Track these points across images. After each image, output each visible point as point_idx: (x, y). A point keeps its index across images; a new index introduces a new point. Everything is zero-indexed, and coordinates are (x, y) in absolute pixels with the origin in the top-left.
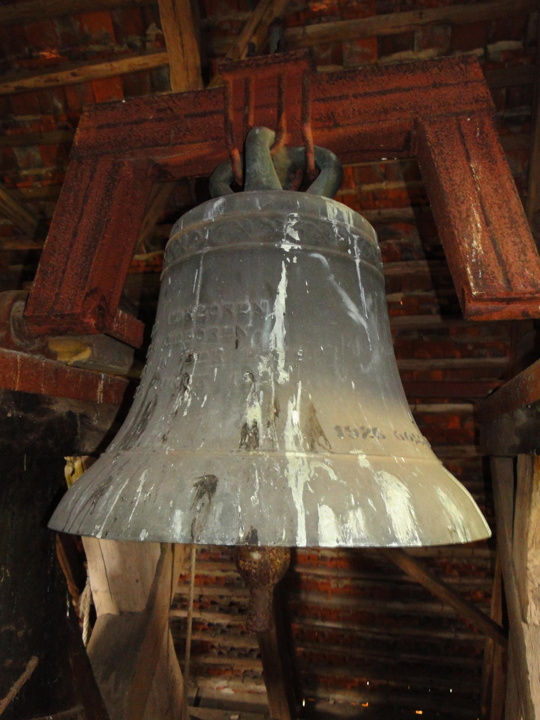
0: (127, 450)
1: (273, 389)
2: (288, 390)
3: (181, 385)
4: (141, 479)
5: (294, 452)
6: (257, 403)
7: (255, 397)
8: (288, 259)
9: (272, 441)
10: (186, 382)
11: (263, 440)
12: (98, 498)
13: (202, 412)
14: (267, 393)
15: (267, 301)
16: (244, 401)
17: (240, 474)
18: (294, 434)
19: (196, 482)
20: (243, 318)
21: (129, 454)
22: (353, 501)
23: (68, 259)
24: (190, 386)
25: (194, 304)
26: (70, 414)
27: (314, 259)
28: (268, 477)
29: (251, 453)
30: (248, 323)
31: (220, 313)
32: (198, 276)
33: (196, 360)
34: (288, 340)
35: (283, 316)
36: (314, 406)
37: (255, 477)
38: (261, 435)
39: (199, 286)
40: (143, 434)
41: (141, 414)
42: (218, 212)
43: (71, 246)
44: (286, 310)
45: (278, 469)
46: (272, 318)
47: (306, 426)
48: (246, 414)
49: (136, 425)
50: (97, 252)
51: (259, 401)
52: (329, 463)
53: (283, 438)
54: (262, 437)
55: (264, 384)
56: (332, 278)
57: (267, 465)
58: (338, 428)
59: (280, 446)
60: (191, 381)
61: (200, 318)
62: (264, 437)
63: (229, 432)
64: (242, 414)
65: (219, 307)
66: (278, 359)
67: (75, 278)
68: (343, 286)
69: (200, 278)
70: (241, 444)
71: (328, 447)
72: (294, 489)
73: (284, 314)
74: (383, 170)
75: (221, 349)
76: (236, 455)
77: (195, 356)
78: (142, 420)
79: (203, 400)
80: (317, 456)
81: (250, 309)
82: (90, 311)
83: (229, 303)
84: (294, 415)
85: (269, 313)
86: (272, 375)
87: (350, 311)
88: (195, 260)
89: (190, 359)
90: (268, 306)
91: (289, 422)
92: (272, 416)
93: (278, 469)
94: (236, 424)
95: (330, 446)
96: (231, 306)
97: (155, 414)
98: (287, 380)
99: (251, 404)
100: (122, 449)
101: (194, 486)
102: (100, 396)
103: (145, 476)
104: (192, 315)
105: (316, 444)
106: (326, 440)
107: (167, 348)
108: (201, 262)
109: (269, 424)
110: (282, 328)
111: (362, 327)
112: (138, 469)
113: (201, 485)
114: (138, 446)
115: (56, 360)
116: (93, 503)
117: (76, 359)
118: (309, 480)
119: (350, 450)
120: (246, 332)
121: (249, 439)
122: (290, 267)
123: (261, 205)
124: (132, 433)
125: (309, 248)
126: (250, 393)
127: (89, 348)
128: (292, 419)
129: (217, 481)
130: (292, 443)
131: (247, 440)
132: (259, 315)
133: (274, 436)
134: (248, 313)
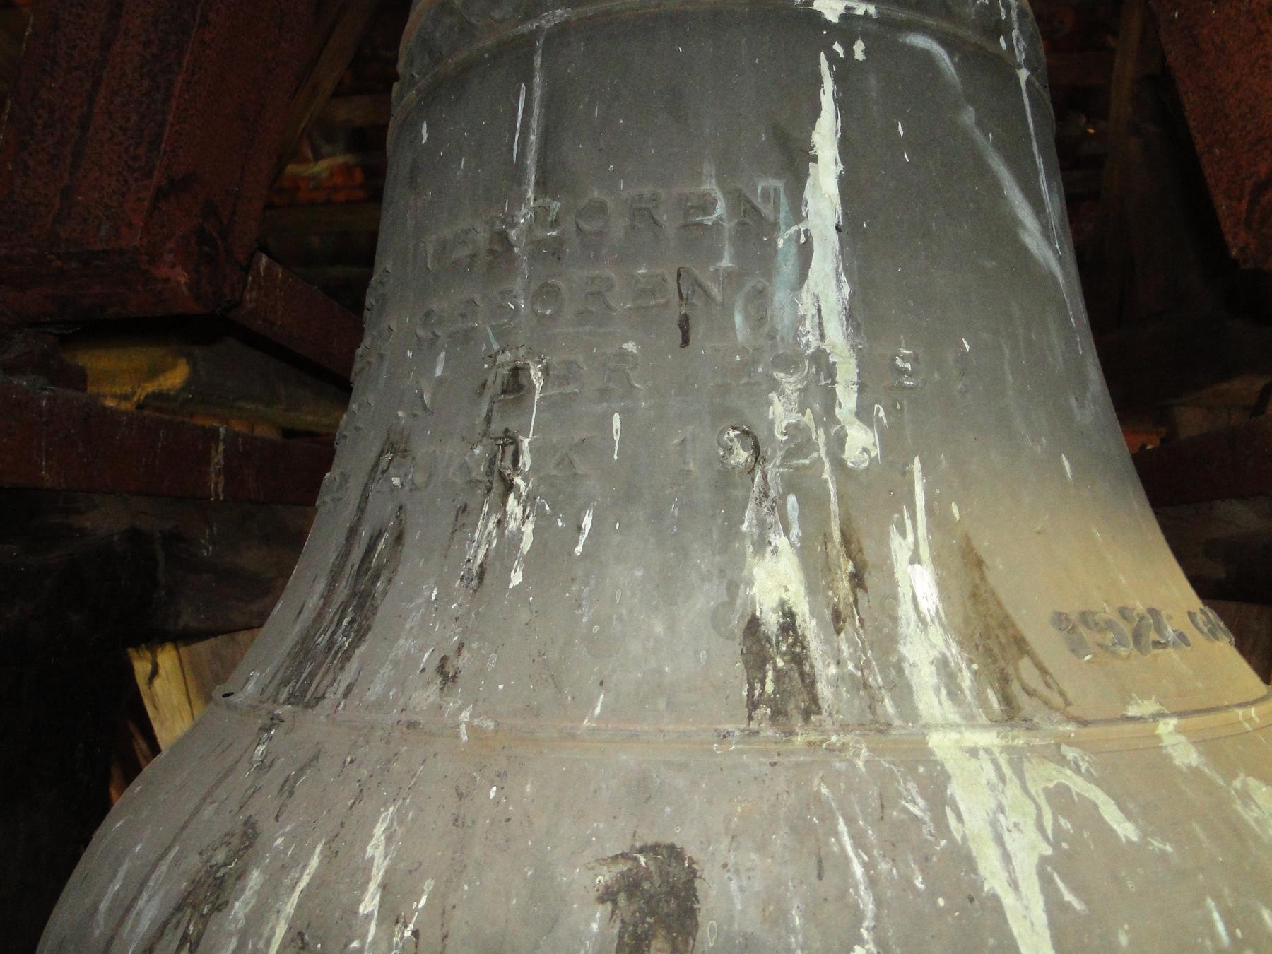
0: (308, 706)
1: (831, 487)
2: (879, 492)
3: (490, 472)
4: (370, 851)
5: (953, 726)
6: (780, 541)
7: (770, 519)
8: (837, 47)
9: (866, 686)
10: (508, 463)
11: (829, 682)
12: (205, 919)
13: (579, 573)
14: (813, 502)
15: (779, 184)
16: (731, 530)
17: (780, 839)
18: (935, 653)
19: (604, 877)
20: (697, 237)
21: (314, 725)
22: (1220, 927)
24: (526, 479)
25: (522, 199)
26: (135, 536)
27: (913, 50)
28: (892, 848)
29: (799, 740)
30: (719, 257)
31: (618, 226)
32: (529, 104)
33: (538, 385)
34: (860, 316)
35: (834, 236)
36: (975, 543)
37: (843, 850)
38: (819, 665)
39: (533, 138)
40: (363, 648)
41: (348, 572)
44: (845, 214)
45: (918, 808)
46: (802, 240)
47: (967, 620)
48: (750, 583)
49: (332, 609)
50: (185, 64)
52: (1084, 767)
53: (900, 671)
54: (825, 671)
55: (797, 468)
56: (969, 116)
57: (873, 792)
58: (1060, 619)
59: (897, 705)
60: (526, 460)
61: (544, 242)
62: (833, 670)
63: (697, 652)
64: (735, 584)
65: (611, 206)
66: (834, 383)
67: (120, 143)
68: (999, 147)
69: (536, 111)
70: (753, 705)
71: (1058, 701)
72: (1008, 899)
73: (838, 229)
75: (630, 347)
76: (741, 752)
77: (536, 374)
78: (353, 595)
79: (579, 528)
80: (1037, 742)
81: (720, 209)
82: (171, 245)
83: (647, 190)
84: (918, 583)
85: (789, 227)
86: (820, 437)
87: (1024, 227)
88: (515, 56)
89: (516, 383)
90: (783, 200)
91: (905, 610)
92: (844, 586)
93: (918, 808)
94: (717, 619)
95: (1062, 693)
96: (655, 199)
97: (401, 579)
98: (875, 452)
99: (762, 544)
100: (287, 701)
101: (602, 900)
102: (216, 484)
103: (389, 840)
104: (513, 234)
105: (1015, 687)
106: (1043, 671)
107: (427, 348)
108: (538, 60)
109: (837, 616)
110: (837, 274)
111: (1054, 277)
112: (358, 799)
113: (630, 896)
114: (345, 696)
115: (84, 390)
116: (185, 937)
117: (150, 388)
118: (1048, 851)
119: (1126, 703)
120: (715, 290)
121: (777, 680)
122: (845, 71)
124: (322, 640)
125: (902, 15)
126: (752, 504)
127: (183, 361)
128: (914, 598)
129: (693, 873)
130: (937, 691)
131: (770, 687)
132: (755, 229)
133: (868, 664)
134: (717, 224)
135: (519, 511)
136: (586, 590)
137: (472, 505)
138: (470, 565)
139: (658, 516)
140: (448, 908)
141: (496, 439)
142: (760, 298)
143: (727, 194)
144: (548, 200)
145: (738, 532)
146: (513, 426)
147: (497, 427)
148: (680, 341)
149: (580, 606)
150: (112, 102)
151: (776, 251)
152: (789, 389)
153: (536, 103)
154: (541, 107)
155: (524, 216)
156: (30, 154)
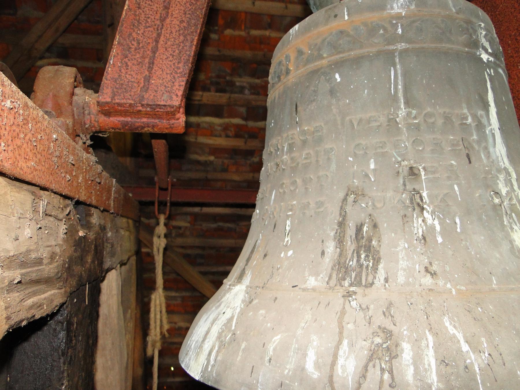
6: (515, 227)
23: (159, 35)
24: (429, 206)
25: (399, 108)
30: (472, 135)
39: (400, 87)
42: (408, 6)
43: (163, 20)
44: (500, 125)
51: (516, 225)
67: (171, 61)
69: (400, 78)
74: (269, 20)
108: (397, 60)
123: (454, 7)
126: (504, 216)
135: (430, 216)
136: (468, 243)
137: (408, 215)
138: (417, 235)
139: (480, 219)
140: (496, 346)
141: (411, 192)
142: (486, 148)
143: (471, 114)
144: (411, 110)
145: (504, 225)
146: (417, 187)
147: (409, 187)
148: (468, 162)
149: (468, 249)
150: (166, 43)
151: (487, 135)
152: (501, 179)
153: (399, 75)
154: (402, 76)
155: (401, 114)
156: (129, 60)
